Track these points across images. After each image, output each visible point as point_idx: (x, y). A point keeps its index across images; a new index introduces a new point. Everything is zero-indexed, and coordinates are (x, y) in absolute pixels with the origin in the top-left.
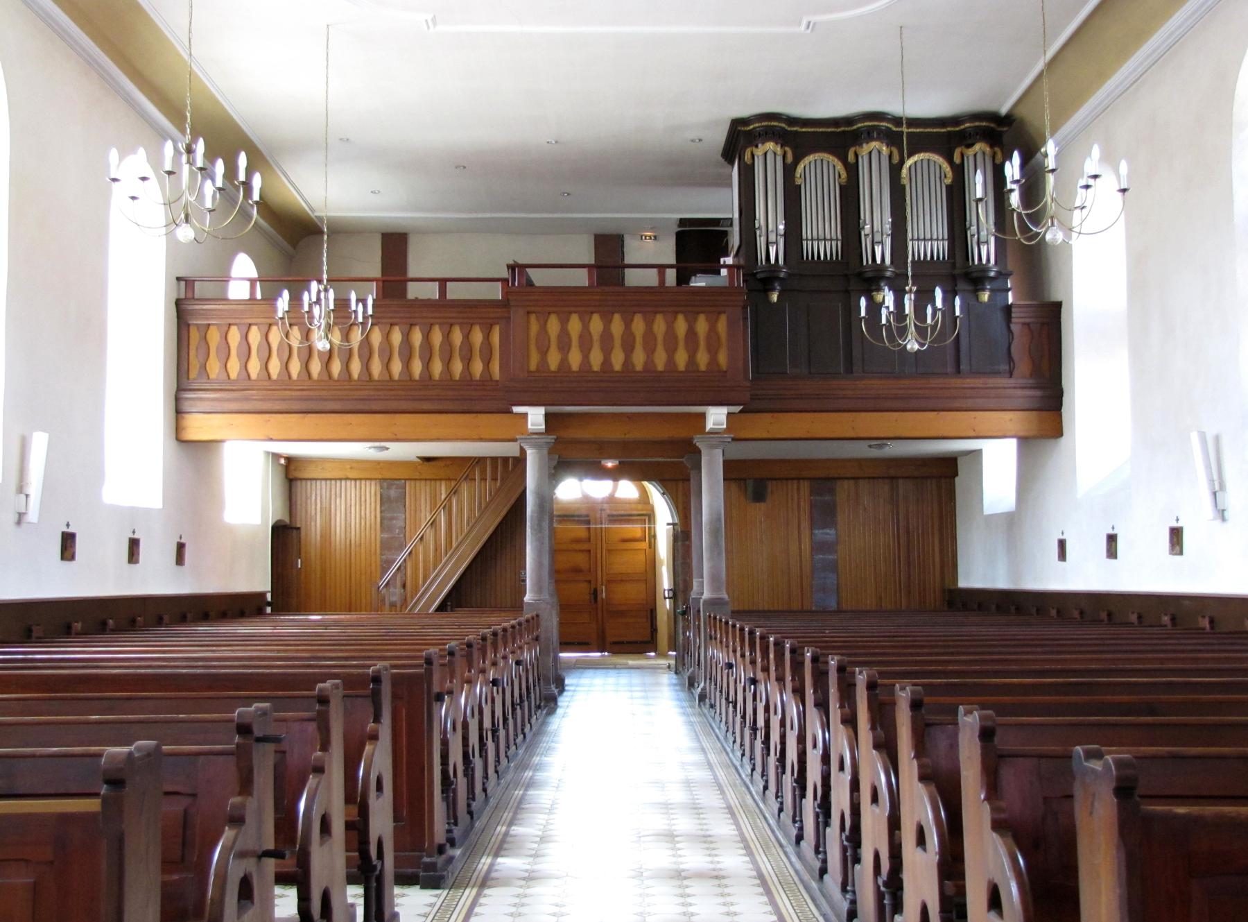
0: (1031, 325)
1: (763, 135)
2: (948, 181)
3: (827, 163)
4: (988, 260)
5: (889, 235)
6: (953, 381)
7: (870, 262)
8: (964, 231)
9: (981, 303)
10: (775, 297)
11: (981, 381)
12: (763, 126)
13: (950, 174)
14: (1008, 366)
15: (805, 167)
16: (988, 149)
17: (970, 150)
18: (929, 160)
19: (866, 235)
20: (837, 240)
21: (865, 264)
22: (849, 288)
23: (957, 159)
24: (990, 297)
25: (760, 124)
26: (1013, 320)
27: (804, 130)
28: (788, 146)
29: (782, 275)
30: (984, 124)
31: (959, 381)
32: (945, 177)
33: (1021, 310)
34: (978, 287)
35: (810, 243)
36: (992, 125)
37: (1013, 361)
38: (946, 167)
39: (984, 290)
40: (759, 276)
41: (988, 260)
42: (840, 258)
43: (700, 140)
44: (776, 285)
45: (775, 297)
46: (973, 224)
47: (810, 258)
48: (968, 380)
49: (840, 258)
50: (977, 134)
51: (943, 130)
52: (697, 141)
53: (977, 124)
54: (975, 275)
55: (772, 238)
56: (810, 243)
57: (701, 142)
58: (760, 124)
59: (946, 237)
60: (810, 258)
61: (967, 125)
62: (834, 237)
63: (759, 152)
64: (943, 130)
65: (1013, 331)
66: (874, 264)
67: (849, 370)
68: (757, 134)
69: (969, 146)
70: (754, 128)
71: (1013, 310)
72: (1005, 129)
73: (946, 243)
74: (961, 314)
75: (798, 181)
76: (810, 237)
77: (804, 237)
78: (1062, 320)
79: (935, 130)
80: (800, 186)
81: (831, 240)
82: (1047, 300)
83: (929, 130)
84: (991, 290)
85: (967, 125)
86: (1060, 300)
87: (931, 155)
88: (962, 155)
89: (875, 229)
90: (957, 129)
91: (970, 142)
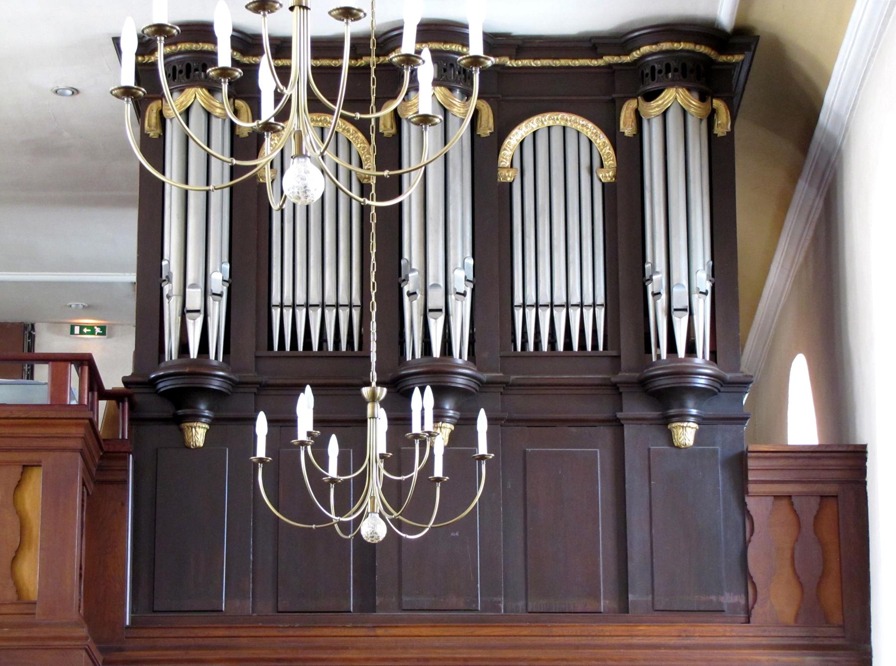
0: (794, 499)
1: (660, 72)
2: (607, 175)
3: (575, 135)
4: (691, 349)
5: (706, 293)
6: (609, 629)
7: (418, 355)
8: (641, 280)
9: (678, 447)
10: (198, 434)
11: (674, 629)
12: (661, 52)
13: (610, 161)
14: (743, 596)
15: (521, 144)
16: (693, 103)
17: (654, 104)
18: (564, 128)
19: (656, 294)
20: (351, 306)
21: (409, 357)
22: (619, 415)
23: (627, 127)
24: (698, 435)
25: (654, 48)
26: (752, 488)
27: (520, 63)
28: (718, 98)
29: (215, 384)
30: (682, 46)
31: (621, 629)
32: (602, 166)
33: (767, 463)
34: (672, 412)
35: (288, 313)
36: (702, 49)
37: (754, 584)
38: (602, 141)
39: (683, 417)
40: (163, 386)
41: (691, 349)
42: (601, 348)
43: (75, 92)
44: (202, 407)
45: (198, 434)
46: (657, 269)
47: (301, 347)
48: (642, 628)
49: (601, 348)
50: (668, 68)
51: (594, 63)
52: (69, 92)
53: (665, 46)
54: (664, 383)
55: (195, 299)
56: (288, 313)
57: (77, 97)
58: (654, 48)
59: (600, 299)
60: (301, 347)
61: (646, 49)
62: (343, 299)
63: (655, 107)
64: (594, 63)
65: (752, 513)
66: (426, 359)
67: (367, 604)
68: (648, 71)
69: (651, 96)
70: (644, 56)
71: (751, 464)
72: (737, 58)
73: (601, 313)
74: (444, 474)
75: (507, 175)
76: (288, 300)
77: (276, 299)
78: (869, 488)
79: (577, 63)
80: (511, 184)
81: (337, 306)
82: (852, 443)
83: (563, 62)
84: (702, 421)
85: (646, 49)
86: (865, 443)
87: (566, 116)
88: (637, 114)
89: (431, 282)
90: (627, 59)
91: (652, 86)
